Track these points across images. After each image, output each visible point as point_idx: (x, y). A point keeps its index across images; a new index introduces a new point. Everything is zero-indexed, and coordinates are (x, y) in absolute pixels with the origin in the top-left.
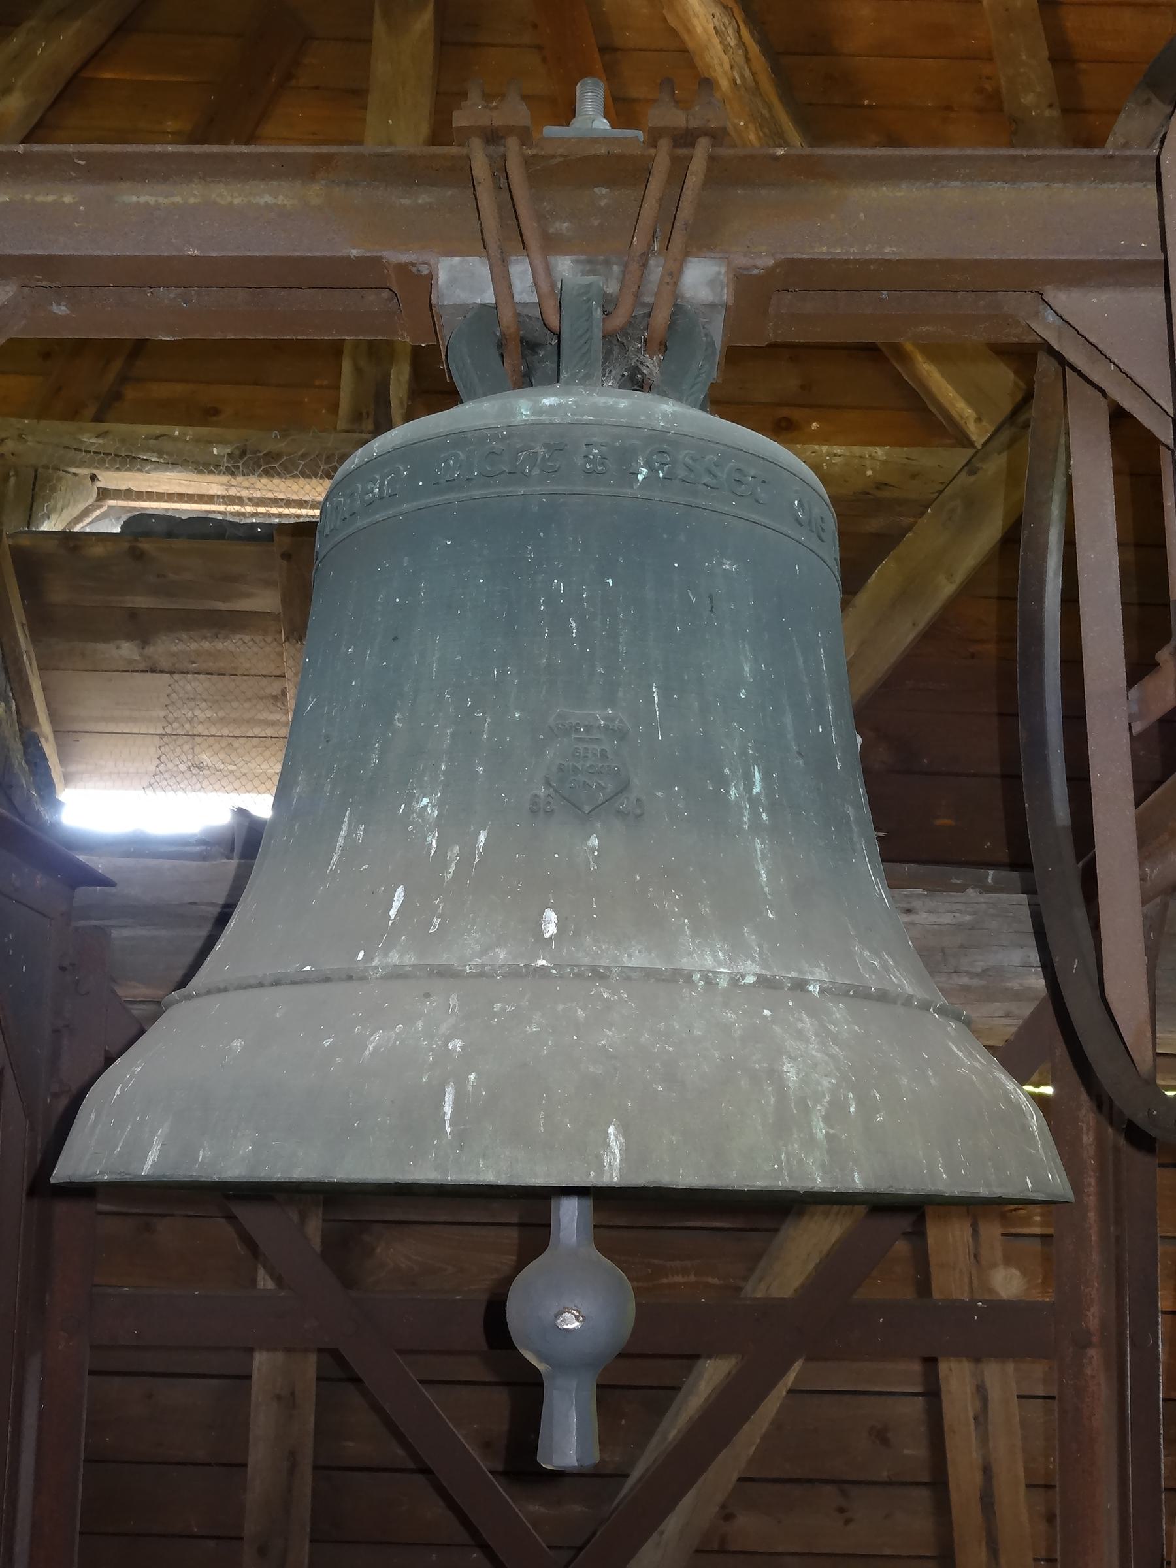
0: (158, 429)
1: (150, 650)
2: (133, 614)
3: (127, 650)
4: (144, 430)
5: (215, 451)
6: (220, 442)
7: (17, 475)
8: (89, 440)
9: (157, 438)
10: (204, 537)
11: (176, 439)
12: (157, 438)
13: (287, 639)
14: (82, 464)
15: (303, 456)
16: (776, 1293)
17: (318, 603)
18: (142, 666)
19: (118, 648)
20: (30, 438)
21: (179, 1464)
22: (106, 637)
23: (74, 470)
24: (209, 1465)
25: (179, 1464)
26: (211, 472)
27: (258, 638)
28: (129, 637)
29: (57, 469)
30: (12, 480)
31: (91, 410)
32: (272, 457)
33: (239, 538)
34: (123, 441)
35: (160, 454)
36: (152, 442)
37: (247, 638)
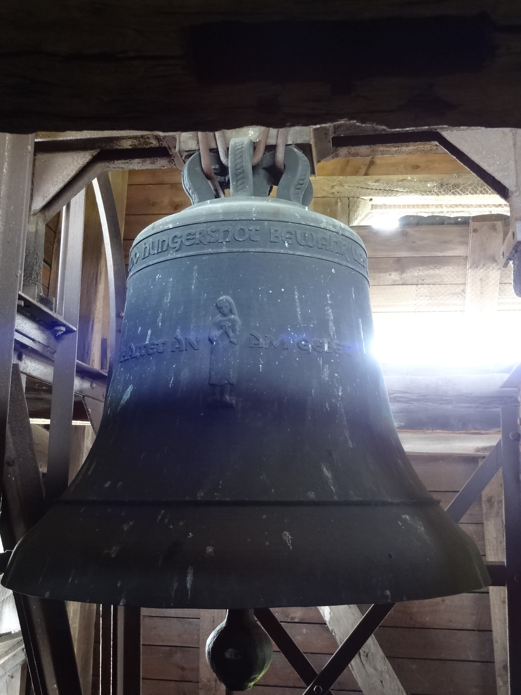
0: (401, 177)
1: (404, 275)
2: (399, 260)
3: (395, 276)
4: (395, 177)
5: (429, 185)
6: (432, 181)
7: (341, 201)
8: (371, 184)
9: (402, 181)
10: (434, 224)
11: (410, 181)
12: (402, 181)
13: (471, 267)
14: (365, 195)
15: (470, 185)
16: (189, 569)
17: (34, 200)
18: (400, 283)
19: (390, 275)
20: (346, 185)
21: (459, 630)
22: (386, 270)
23: (363, 197)
24: (474, 630)
25: (459, 630)
26: (428, 195)
27: (456, 268)
28: (396, 270)
29: (358, 198)
30: (339, 204)
31: (363, 171)
32: (456, 186)
33: (451, 224)
34: (387, 183)
35: (404, 188)
36: (400, 183)
37: (450, 268)
